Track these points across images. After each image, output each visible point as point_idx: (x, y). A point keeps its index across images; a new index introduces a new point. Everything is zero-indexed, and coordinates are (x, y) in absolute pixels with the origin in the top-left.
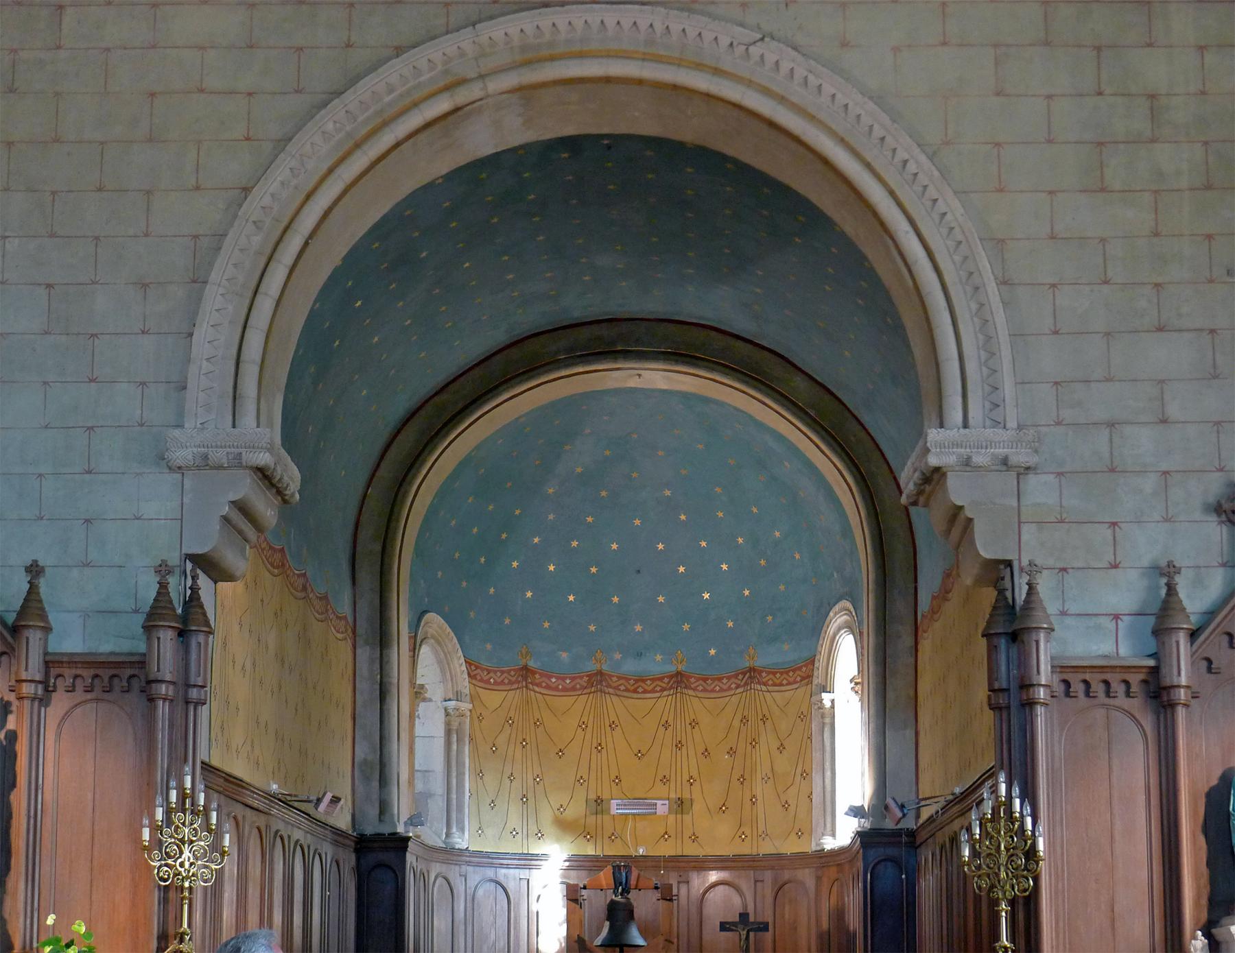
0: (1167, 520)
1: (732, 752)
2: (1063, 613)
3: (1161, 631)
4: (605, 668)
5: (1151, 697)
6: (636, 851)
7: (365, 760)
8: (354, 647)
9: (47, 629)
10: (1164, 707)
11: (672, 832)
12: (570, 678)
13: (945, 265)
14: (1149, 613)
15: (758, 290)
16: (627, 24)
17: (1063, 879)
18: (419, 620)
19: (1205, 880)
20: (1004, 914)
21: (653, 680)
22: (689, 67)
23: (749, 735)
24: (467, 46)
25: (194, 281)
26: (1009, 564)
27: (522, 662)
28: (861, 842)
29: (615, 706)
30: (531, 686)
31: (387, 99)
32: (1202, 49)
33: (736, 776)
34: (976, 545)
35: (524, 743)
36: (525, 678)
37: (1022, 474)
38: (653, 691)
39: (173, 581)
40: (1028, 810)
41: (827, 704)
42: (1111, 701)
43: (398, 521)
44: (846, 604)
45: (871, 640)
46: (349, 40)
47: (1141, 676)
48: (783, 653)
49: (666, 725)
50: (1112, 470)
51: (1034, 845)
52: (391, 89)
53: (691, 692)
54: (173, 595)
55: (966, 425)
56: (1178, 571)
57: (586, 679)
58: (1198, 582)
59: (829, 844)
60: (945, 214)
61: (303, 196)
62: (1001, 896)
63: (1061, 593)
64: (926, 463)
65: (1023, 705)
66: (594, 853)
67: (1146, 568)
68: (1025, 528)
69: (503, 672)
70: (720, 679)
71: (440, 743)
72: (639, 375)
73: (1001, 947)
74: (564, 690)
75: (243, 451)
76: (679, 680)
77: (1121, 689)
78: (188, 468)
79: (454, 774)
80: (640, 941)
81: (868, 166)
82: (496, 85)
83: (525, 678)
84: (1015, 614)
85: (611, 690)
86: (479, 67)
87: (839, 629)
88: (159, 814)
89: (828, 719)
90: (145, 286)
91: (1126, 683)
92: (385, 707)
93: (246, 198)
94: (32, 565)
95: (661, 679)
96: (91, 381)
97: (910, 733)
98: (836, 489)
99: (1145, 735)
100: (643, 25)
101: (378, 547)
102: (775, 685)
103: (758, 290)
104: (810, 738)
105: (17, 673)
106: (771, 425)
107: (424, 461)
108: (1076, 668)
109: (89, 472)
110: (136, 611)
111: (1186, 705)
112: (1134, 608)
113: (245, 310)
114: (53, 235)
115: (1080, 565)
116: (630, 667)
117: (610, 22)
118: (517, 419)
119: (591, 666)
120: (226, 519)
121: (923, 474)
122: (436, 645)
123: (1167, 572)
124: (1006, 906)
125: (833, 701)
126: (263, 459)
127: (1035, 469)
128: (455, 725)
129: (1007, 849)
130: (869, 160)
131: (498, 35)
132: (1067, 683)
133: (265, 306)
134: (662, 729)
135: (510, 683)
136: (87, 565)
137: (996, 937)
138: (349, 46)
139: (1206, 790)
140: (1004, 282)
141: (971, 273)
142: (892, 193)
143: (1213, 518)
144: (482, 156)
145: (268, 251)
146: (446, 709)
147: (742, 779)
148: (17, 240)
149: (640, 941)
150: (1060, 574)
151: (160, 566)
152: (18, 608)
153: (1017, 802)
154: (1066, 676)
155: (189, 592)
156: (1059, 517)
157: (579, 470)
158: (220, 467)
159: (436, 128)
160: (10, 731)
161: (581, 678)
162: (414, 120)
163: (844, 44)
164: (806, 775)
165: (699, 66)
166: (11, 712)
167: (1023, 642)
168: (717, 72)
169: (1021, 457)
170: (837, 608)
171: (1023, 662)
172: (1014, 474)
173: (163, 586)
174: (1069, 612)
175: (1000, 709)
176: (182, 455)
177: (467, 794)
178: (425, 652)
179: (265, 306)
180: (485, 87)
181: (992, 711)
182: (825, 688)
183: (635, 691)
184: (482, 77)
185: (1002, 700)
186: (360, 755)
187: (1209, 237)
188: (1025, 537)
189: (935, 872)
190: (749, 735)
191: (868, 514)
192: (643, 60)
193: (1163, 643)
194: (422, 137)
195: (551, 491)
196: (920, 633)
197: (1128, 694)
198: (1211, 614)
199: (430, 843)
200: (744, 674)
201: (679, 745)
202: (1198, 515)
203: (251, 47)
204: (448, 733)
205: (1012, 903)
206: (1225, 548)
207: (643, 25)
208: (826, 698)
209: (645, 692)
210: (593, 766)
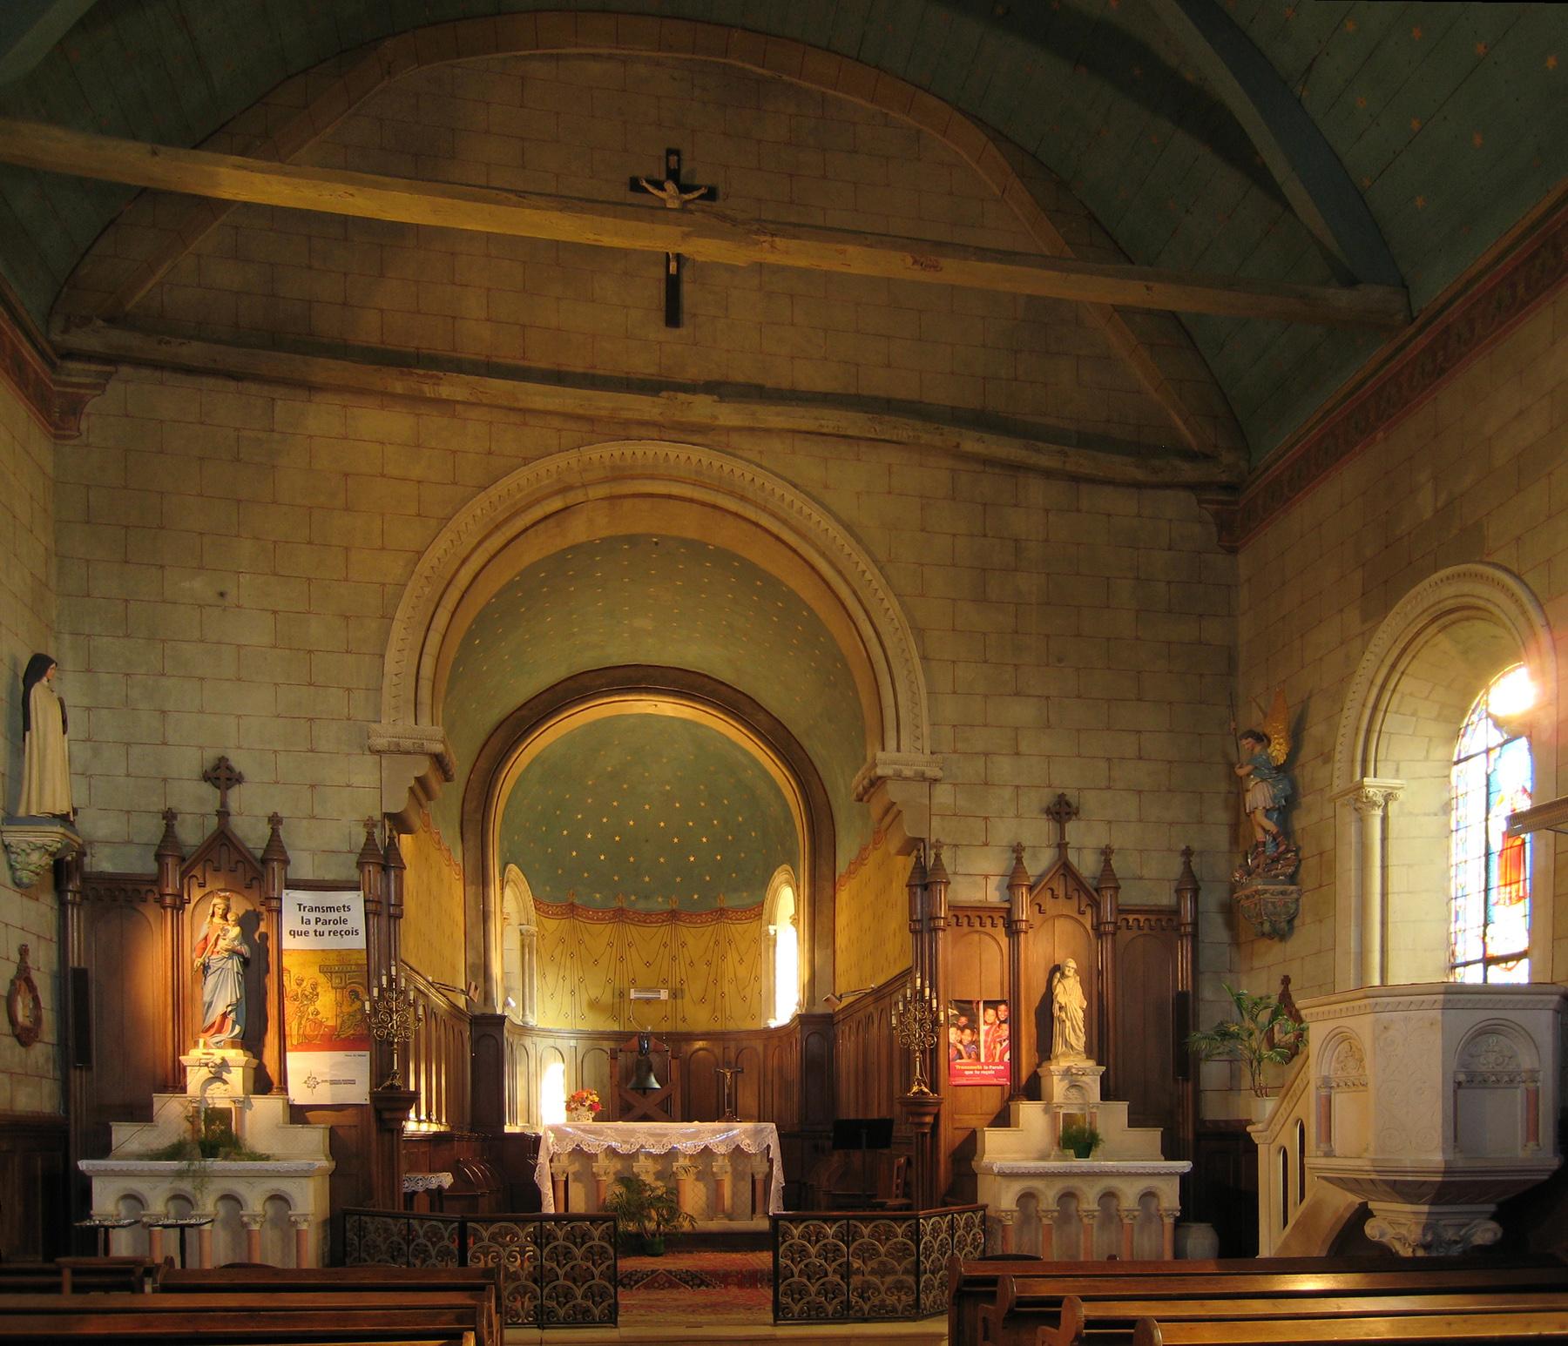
0: (1017, 816)
1: (709, 963)
2: (955, 873)
3: (1011, 887)
4: (625, 906)
6: (646, 1028)
7: (473, 963)
8: (464, 885)
9: (286, 862)
11: (669, 1015)
12: (602, 912)
13: (887, 644)
15: (741, 652)
16: (683, 457)
18: (505, 869)
21: (657, 915)
22: (723, 493)
23: (625, 965)
24: (573, 462)
25: (383, 617)
26: (923, 840)
27: (571, 900)
28: (800, 1021)
29: (633, 932)
30: (576, 917)
31: (518, 496)
32: (1047, 511)
33: (711, 979)
35: (572, 955)
36: (572, 911)
38: (657, 922)
39: (377, 832)
40: (934, 995)
41: (772, 932)
42: (983, 929)
43: (492, 798)
44: (786, 867)
45: (805, 890)
46: (490, 449)
48: (744, 898)
49: (665, 945)
50: (986, 784)
51: (938, 1016)
52: (520, 489)
53: (681, 923)
54: (378, 841)
55: (898, 750)
56: (1024, 849)
57: (612, 913)
58: (1034, 856)
59: (773, 1024)
60: (888, 609)
61: (459, 562)
64: (875, 773)
66: (618, 1029)
68: (933, 818)
69: (557, 907)
70: (701, 915)
71: (518, 953)
72: (656, 705)
74: (598, 919)
75: (425, 742)
76: (673, 916)
77: (989, 922)
78: (384, 752)
79: (527, 975)
80: (657, 1086)
81: (840, 573)
82: (594, 493)
83: (572, 911)
84: (926, 873)
85: (629, 921)
86: (582, 478)
87: (781, 883)
88: (375, 992)
89: (772, 942)
90: (347, 618)
91: (980, 917)
92: (486, 928)
93: (419, 560)
94: (273, 816)
95: (662, 914)
96: (310, 685)
97: (830, 951)
98: (784, 790)
99: (1001, 950)
100: (694, 460)
101: (479, 817)
102: (737, 919)
103: (741, 652)
104: (760, 955)
105: (266, 893)
106: (742, 744)
107: (510, 757)
108: (962, 908)
109: (312, 751)
110: (350, 852)
111: (1026, 932)
113: (422, 640)
114: (275, 574)
116: (641, 905)
117: (672, 456)
118: (572, 731)
119: (615, 904)
120: (411, 789)
121: (871, 780)
122: (514, 886)
125: (775, 931)
126: (438, 748)
127: (940, 780)
128: (527, 942)
130: (841, 569)
131: (595, 457)
133: (434, 638)
134: (662, 948)
135: (562, 914)
136: (314, 817)
138: (490, 453)
140: (924, 658)
141: (904, 650)
142: (855, 593)
143: (1045, 816)
145: (436, 599)
146: (521, 931)
147: (715, 982)
148: (248, 576)
149: (657, 1086)
151: (368, 820)
152: (264, 846)
153: (927, 991)
154: (956, 913)
155: (387, 840)
157: (609, 769)
158: (408, 753)
159: (551, 521)
160: (263, 933)
161: (609, 912)
162: (537, 512)
163: (826, 487)
164: (757, 979)
165: (731, 493)
166: (263, 919)
167: (932, 890)
168: (743, 498)
169: (931, 772)
170: (780, 869)
171: (930, 903)
172: (928, 784)
173: (370, 836)
176: (380, 742)
177: (536, 989)
178: (508, 891)
179: (434, 638)
180: (587, 494)
182: (771, 922)
183: (645, 922)
184: (584, 486)
186: (470, 960)
187: (1047, 636)
188: (933, 824)
189: (853, 1038)
190: (625, 965)
191: (488, 823)
192: (694, 485)
193: (1014, 893)
194: (542, 526)
195: (590, 783)
196: (837, 887)
198: (1041, 876)
199: (516, 1022)
200: (717, 912)
201: (674, 958)
203: (419, 446)
204: (523, 946)
205: (923, 1052)
207: (694, 460)
208: (771, 929)
209: (651, 922)
210: (618, 972)
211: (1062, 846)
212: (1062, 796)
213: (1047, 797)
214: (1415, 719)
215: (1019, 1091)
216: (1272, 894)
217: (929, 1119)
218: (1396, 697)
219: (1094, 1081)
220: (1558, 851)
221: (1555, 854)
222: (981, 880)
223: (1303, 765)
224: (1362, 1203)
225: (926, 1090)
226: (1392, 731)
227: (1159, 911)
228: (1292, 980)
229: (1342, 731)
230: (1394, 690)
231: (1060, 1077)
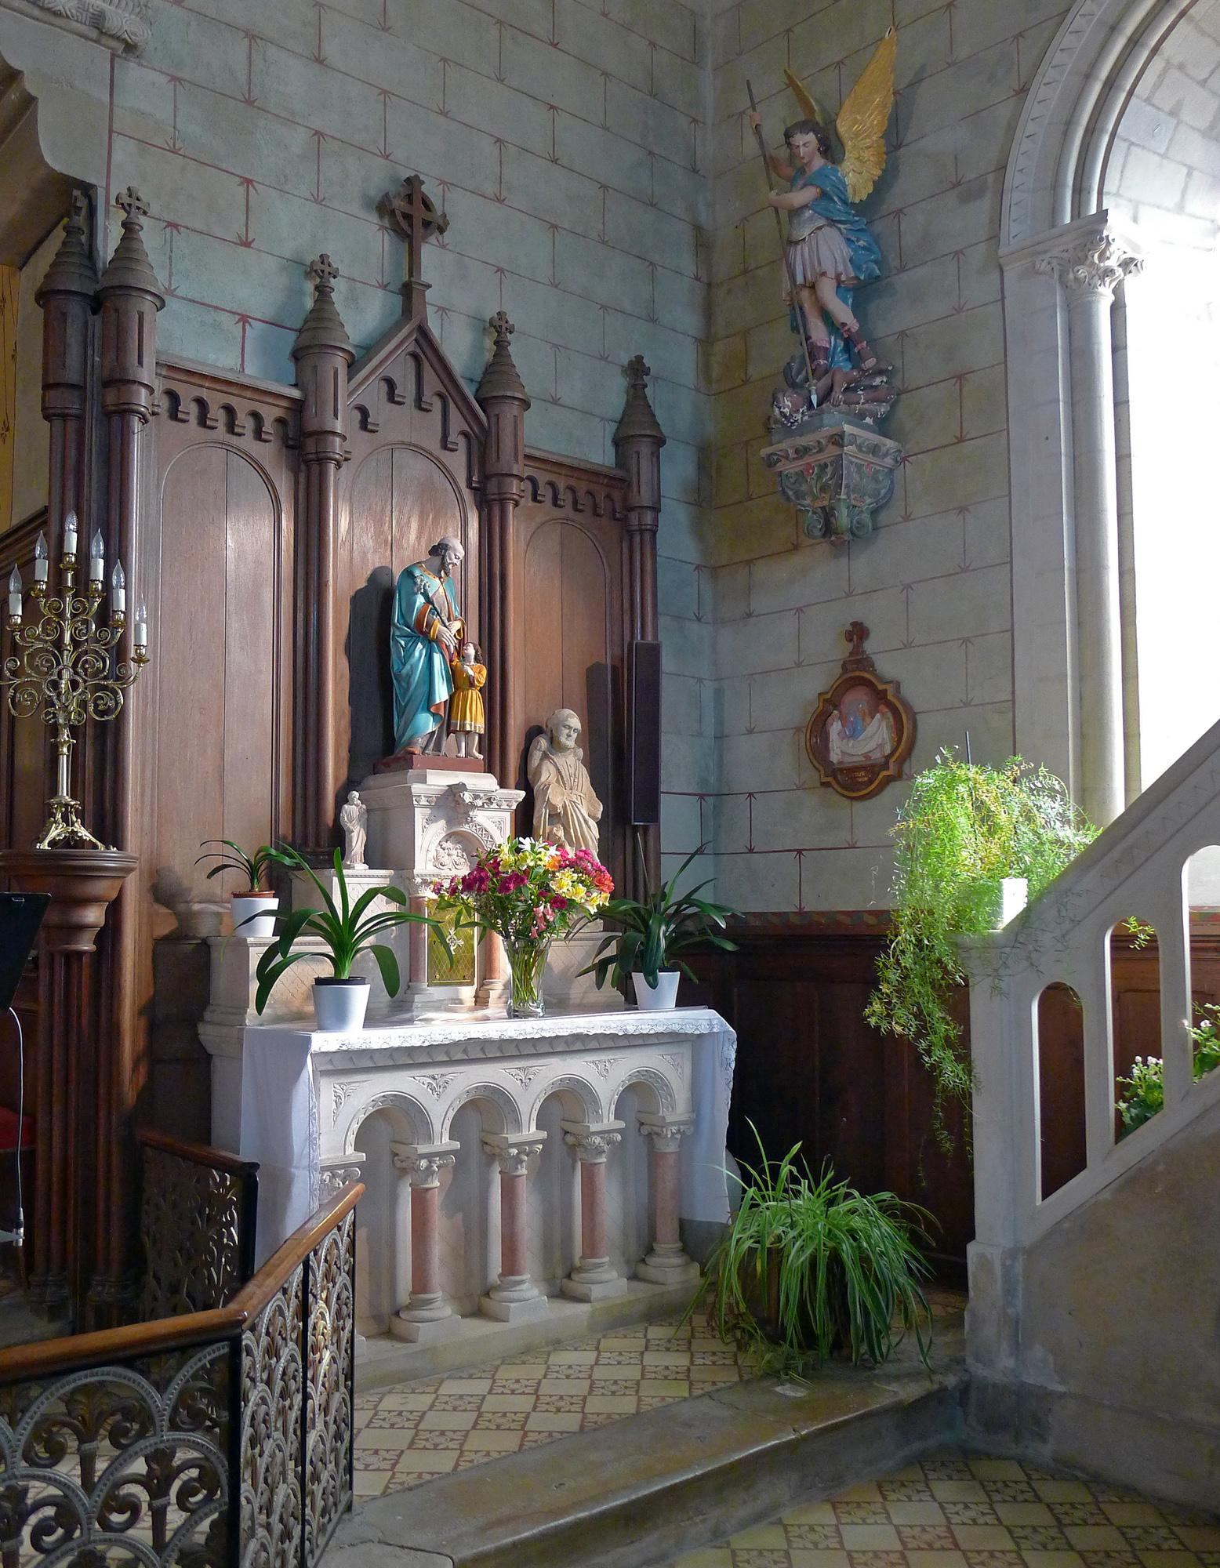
0: (318, 201)
5: (288, 447)
10: (307, 462)
14: (288, 325)
17: (154, 702)
19: (347, 719)
20: (65, 750)
34: (38, 144)
37: (119, 56)
42: (234, 440)
47: (278, 413)
62: (61, 721)
63: (168, 261)
65: (108, 415)
67: (288, 260)
68: (119, 142)
73: (60, 804)
112: (268, 313)
115: (199, 226)
123: (320, 273)
124: (68, 736)
129: (76, 643)
132: (173, 396)
137: (54, 790)
139: (352, 594)
143: (374, 218)
144: (293, 1105)
150: (168, 230)
156: (171, 143)
174: (178, 292)
175: (64, 417)
181: (47, 424)
185: (69, 402)
188: (118, 156)
197: (258, 434)
202: (355, 208)
205: (74, 731)
206: (386, 264)
211: (409, 292)
212: (412, 183)
213: (379, 178)
214: (1173, 121)
215: (318, 844)
216: (859, 448)
217: (94, 915)
218: (1157, 64)
219: (499, 824)
220: (1008, 566)
221: (1011, 562)
222: (229, 322)
223: (899, 212)
224: (92, 1440)
225: (84, 833)
226: (1133, 139)
227: (593, 474)
228: (872, 635)
229: (1031, 128)
230: (1155, 51)
231: (428, 811)
